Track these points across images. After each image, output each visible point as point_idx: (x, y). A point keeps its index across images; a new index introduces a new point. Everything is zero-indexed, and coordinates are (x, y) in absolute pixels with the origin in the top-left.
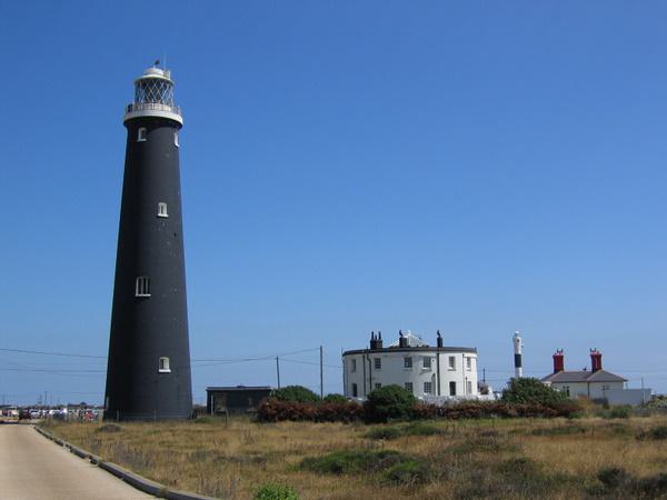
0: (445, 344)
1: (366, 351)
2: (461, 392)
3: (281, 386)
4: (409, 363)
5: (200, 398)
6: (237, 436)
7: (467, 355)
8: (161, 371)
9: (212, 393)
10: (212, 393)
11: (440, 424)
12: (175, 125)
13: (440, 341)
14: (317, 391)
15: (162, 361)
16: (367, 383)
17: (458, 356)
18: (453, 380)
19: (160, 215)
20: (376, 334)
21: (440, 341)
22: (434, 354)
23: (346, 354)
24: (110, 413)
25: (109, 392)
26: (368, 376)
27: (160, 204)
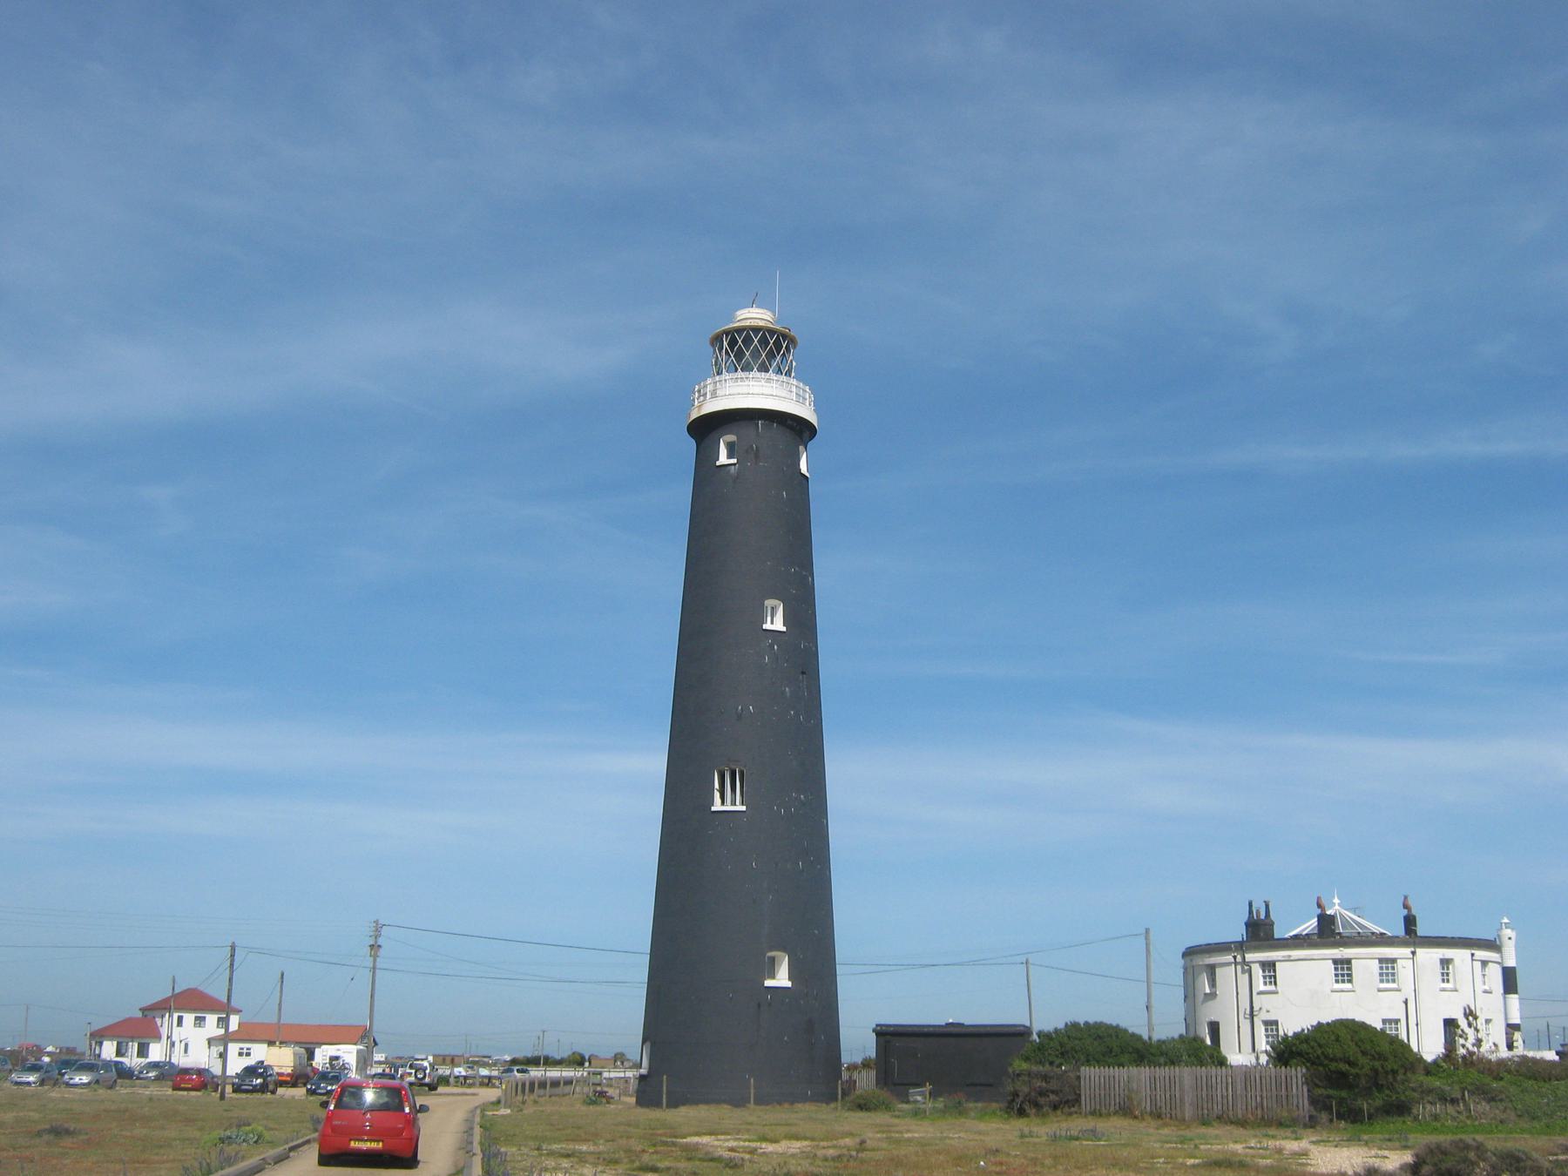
0: (1422, 930)
1: (1241, 947)
2: (1485, 1048)
3: (285, 1020)
4: (1343, 969)
5: (856, 1041)
6: (923, 1128)
7: (1481, 954)
8: (768, 983)
9: (887, 1036)
10: (887, 1036)
11: (1140, 1076)
12: (799, 429)
13: (1410, 921)
14: (1146, 1037)
15: (773, 959)
16: (1245, 1025)
17: (1460, 956)
18: (1213, 1018)
19: (768, 626)
20: (1259, 906)
21: (1410, 921)
22: (1407, 951)
23: (1190, 953)
24: (647, 1092)
25: (652, 1033)
26: (1245, 1005)
27: (769, 603)
